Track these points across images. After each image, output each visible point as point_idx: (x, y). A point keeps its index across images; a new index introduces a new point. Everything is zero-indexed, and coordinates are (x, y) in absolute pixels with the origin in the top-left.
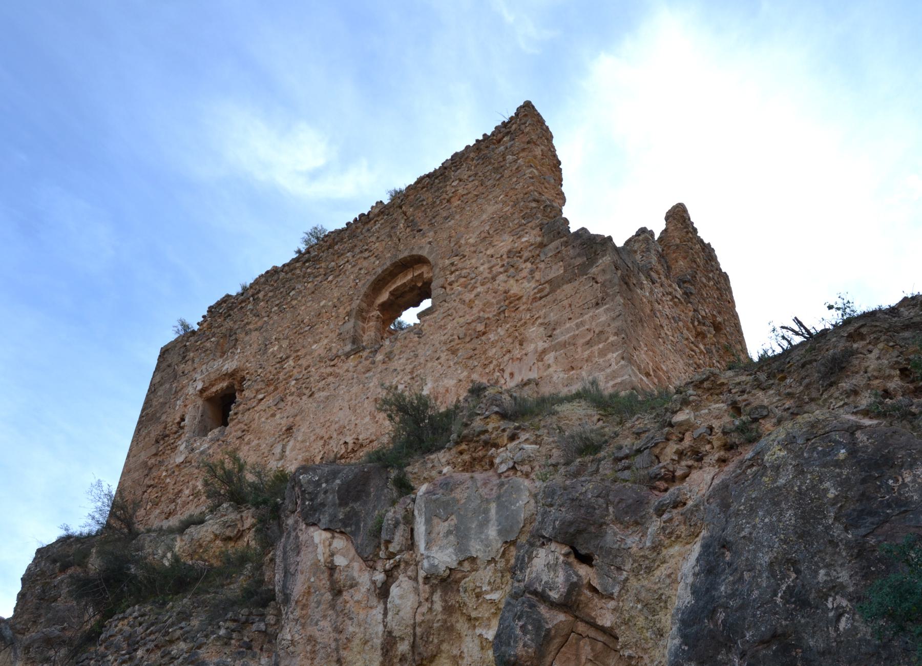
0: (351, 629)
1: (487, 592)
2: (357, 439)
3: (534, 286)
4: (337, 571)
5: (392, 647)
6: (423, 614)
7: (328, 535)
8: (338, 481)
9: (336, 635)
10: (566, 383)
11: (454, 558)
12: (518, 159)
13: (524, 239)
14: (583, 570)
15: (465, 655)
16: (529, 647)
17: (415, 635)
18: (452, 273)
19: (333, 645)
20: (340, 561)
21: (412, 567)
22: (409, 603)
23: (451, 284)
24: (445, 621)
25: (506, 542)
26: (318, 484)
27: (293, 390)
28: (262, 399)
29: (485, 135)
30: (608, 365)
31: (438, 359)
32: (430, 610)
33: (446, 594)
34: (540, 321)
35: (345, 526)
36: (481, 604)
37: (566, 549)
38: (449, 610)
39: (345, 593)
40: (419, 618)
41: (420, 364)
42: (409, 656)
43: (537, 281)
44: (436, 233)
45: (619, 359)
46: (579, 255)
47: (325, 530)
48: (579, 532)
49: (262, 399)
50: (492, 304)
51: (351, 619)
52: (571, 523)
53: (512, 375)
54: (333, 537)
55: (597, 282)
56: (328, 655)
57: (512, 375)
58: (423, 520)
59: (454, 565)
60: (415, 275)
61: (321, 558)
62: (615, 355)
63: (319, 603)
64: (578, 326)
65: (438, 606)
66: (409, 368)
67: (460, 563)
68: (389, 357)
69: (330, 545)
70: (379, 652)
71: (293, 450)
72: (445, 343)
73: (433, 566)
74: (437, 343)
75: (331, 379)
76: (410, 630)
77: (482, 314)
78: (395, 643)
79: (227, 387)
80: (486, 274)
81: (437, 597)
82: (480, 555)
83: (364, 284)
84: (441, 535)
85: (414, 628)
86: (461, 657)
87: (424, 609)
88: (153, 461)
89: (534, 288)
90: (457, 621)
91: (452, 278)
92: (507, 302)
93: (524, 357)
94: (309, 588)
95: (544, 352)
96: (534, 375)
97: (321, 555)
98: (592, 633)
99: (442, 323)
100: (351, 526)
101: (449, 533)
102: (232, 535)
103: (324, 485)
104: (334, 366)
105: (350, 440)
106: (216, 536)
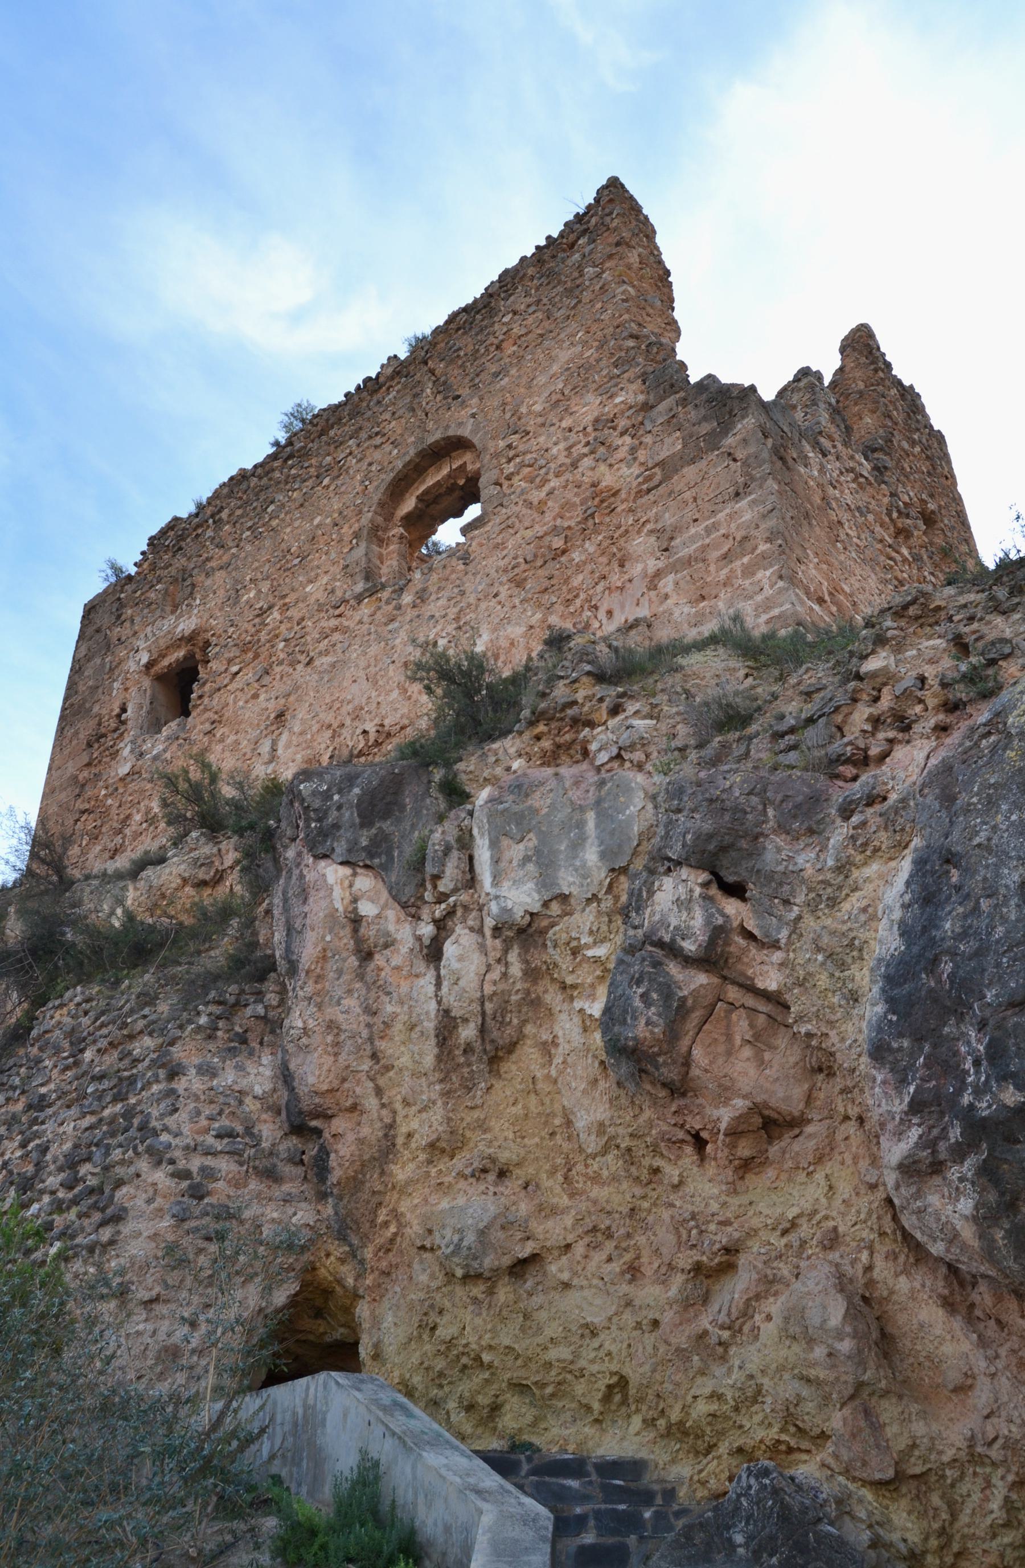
0: (389, 1009)
1: (587, 946)
2: (382, 725)
3: (637, 472)
4: (364, 924)
5: (450, 1033)
6: (495, 983)
7: (347, 871)
8: (357, 791)
9: (368, 1019)
10: (693, 621)
11: (536, 896)
12: (603, 272)
13: (618, 400)
14: (732, 907)
15: (561, 1040)
16: (656, 1025)
17: (483, 1014)
18: (509, 461)
19: (365, 1033)
20: (367, 909)
21: (474, 914)
22: (473, 968)
23: (509, 478)
24: (528, 992)
25: (613, 870)
26: (327, 796)
27: (282, 656)
28: (237, 673)
29: (549, 238)
30: (758, 589)
31: (496, 595)
32: (505, 975)
33: (527, 951)
34: (649, 527)
35: (372, 856)
36: (580, 964)
37: (704, 876)
38: (532, 974)
39: (377, 956)
40: (488, 989)
41: (469, 605)
42: (478, 1046)
43: (642, 464)
44: (481, 399)
45: (774, 578)
46: (705, 419)
47: (342, 863)
48: (723, 849)
49: (237, 673)
50: (574, 505)
51: (389, 993)
52: (710, 837)
53: (610, 613)
54: (355, 874)
55: (735, 460)
56: (359, 1048)
57: (610, 613)
58: (487, 842)
59: (536, 907)
60: (454, 467)
61: (339, 905)
62: (768, 573)
63: (340, 972)
64: (708, 531)
65: (516, 970)
66: (452, 612)
67: (546, 904)
68: (422, 596)
69: (351, 886)
70: (433, 1041)
71: (287, 746)
72: (505, 571)
73: (505, 910)
74: (493, 572)
75: (337, 637)
76: (476, 1007)
77: (559, 521)
78: (456, 1027)
79: (185, 658)
80: (562, 459)
81: (513, 957)
82: (575, 890)
83: (377, 488)
84: (515, 863)
85: (482, 1004)
86: (555, 1043)
87: (495, 975)
88: (85, 774)
89: (638, 477)
90: (546, 992)
91: (510, 468)
92: (597, 499)
93: (628, 585)
94: (324, 950)
95: (658, 574)
96: (643, 612)
97: (339, 900)
98: (750, 1001)
99: (499, 540)
100: (379, 856)
101: (527, 859)
102: (207, 878)
103: (336, 797)
104: (340, 616)
105: (371, 727)
106: (185, 881)
